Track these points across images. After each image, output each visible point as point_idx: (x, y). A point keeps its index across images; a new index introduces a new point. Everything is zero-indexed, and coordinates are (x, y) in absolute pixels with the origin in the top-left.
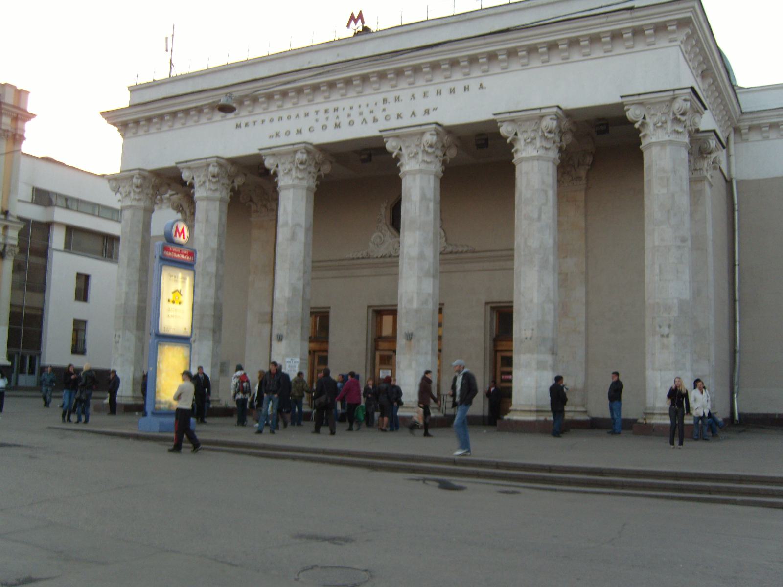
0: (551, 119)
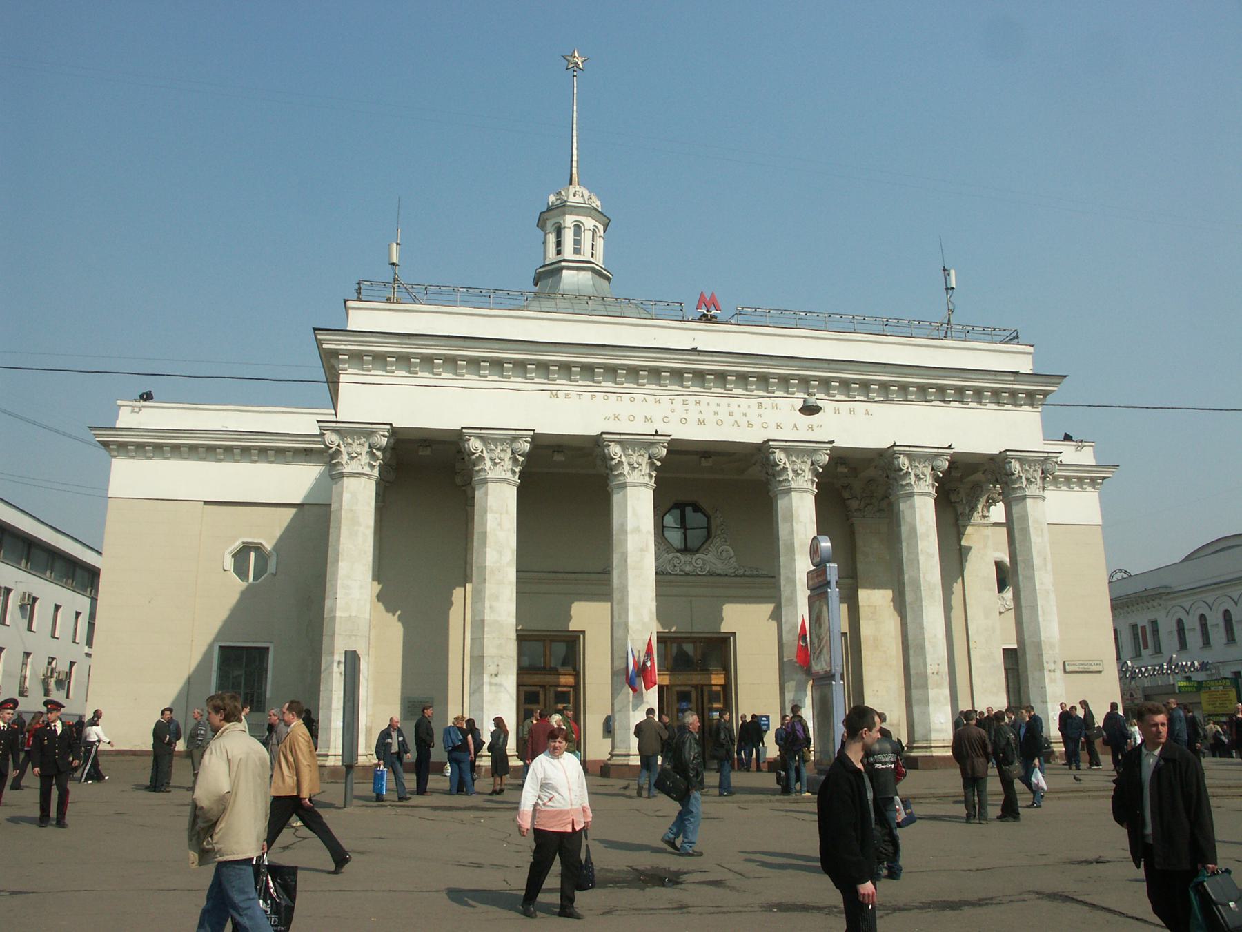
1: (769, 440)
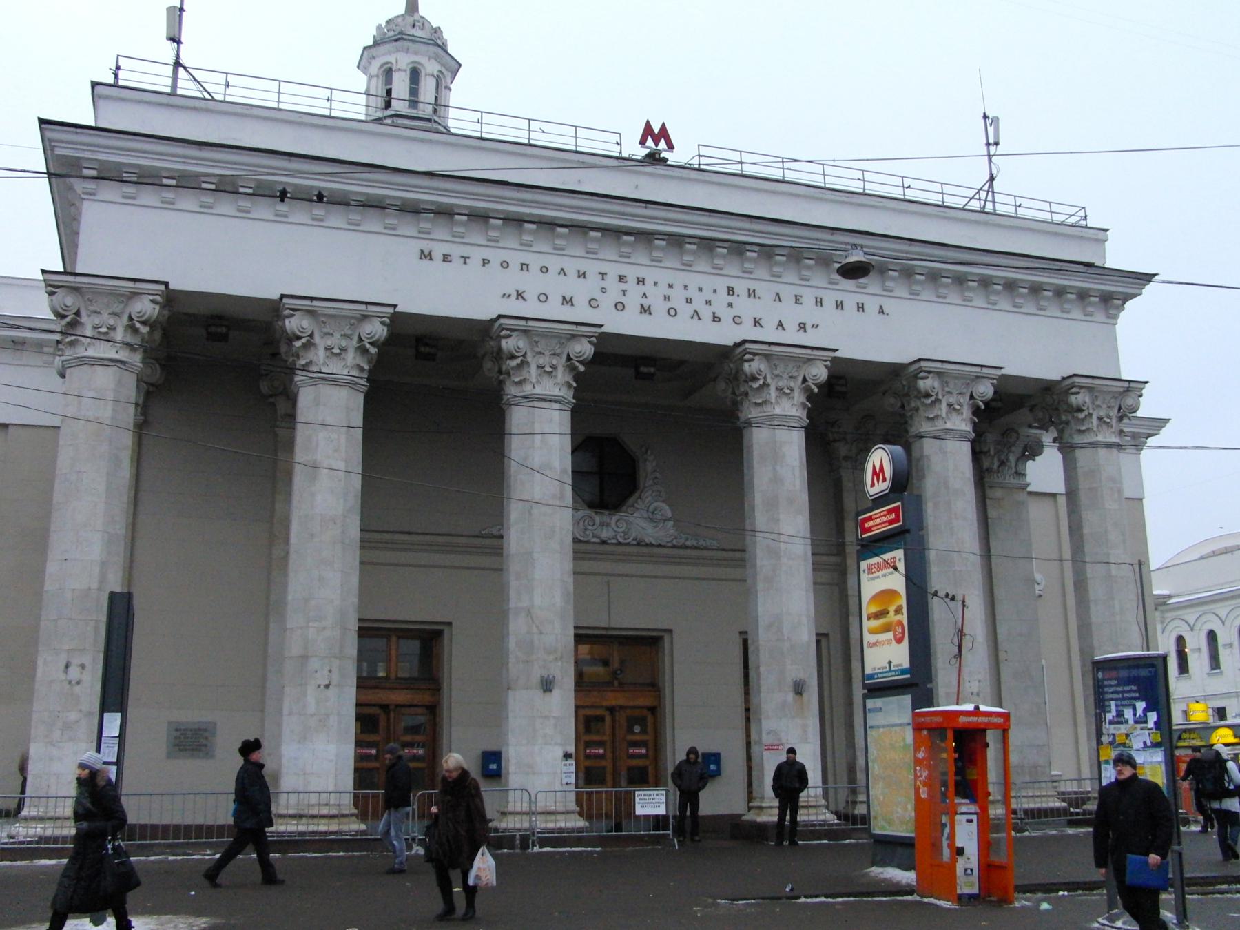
0: (152, 301)
1: (745, 341)
